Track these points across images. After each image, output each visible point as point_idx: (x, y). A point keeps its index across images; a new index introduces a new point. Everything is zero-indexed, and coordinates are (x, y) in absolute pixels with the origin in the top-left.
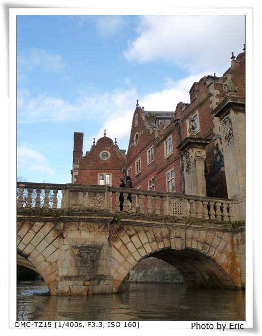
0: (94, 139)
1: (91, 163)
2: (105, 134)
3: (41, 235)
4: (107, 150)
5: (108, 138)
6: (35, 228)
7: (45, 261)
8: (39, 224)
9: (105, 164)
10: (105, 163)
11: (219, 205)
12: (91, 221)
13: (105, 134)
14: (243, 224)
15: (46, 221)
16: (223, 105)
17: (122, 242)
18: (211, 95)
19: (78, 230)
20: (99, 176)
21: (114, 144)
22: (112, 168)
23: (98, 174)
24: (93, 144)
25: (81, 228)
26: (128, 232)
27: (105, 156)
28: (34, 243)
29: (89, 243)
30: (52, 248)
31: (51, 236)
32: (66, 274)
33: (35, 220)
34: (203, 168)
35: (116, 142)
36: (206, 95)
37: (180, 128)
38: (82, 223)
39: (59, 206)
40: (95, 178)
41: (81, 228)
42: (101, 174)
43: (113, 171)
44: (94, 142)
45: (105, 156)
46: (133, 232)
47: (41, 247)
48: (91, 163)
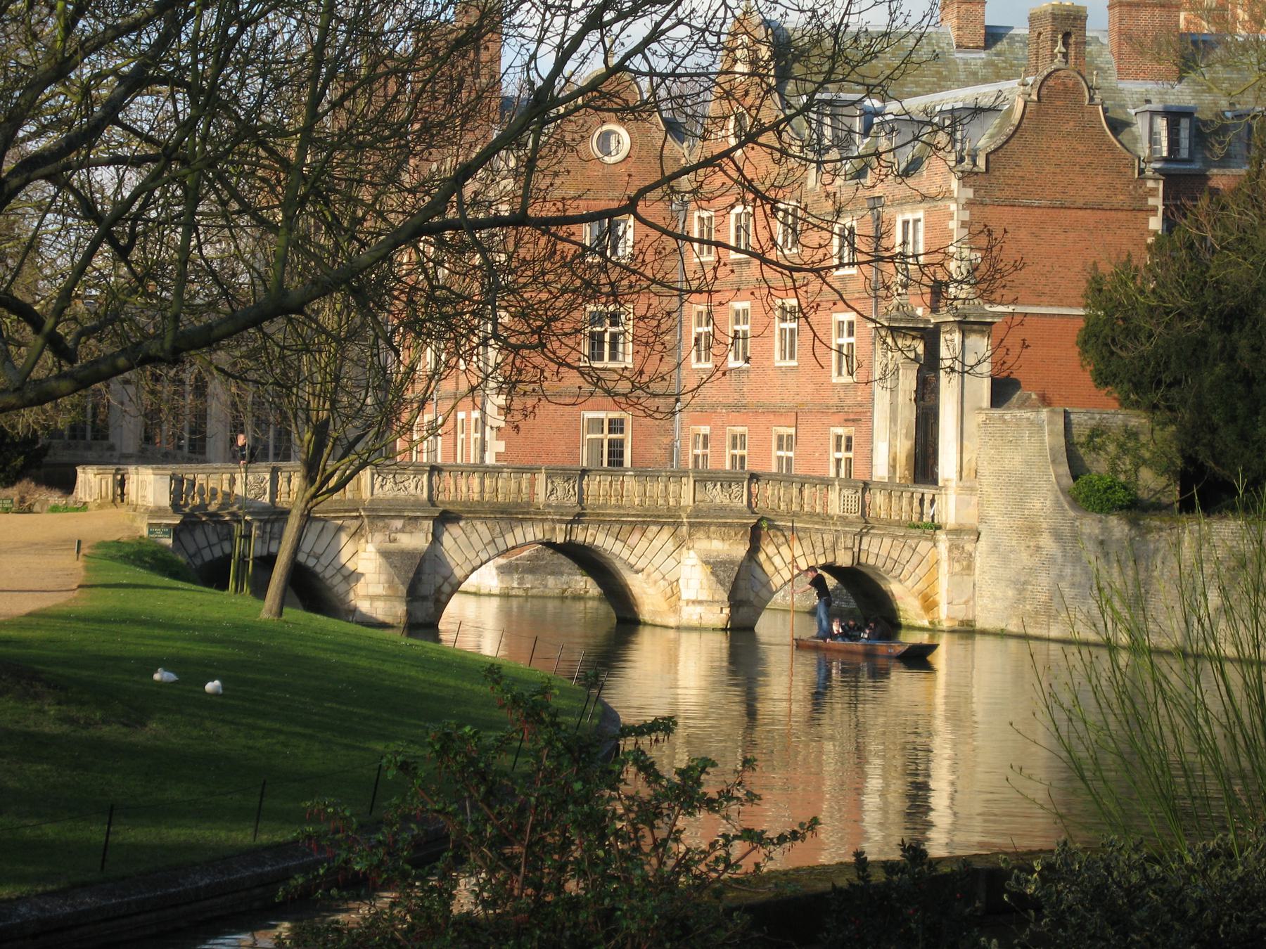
3: (657, 543)
6: (650, 535)
7: (664, 578)
8: (654, 529)
11: (917, 496)
14: (30, 510)
15: (663, 525)
17: (261, 802)
26: (775, 540)
28: (649, 555)
29: (723, 557)
30: (671, 562)
31: (670, 546)
32: (694, 598)
33: (648, 524)
34: (681, 667)
39: (472, 461)
47: (657, 561)
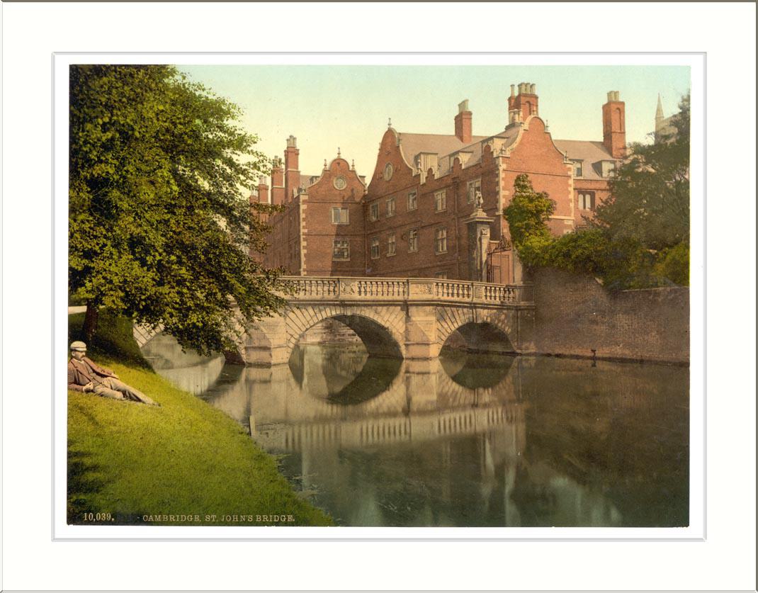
2: (339, 154)
13: (339, 154)
35: (353, 166)
44: (325, 165)
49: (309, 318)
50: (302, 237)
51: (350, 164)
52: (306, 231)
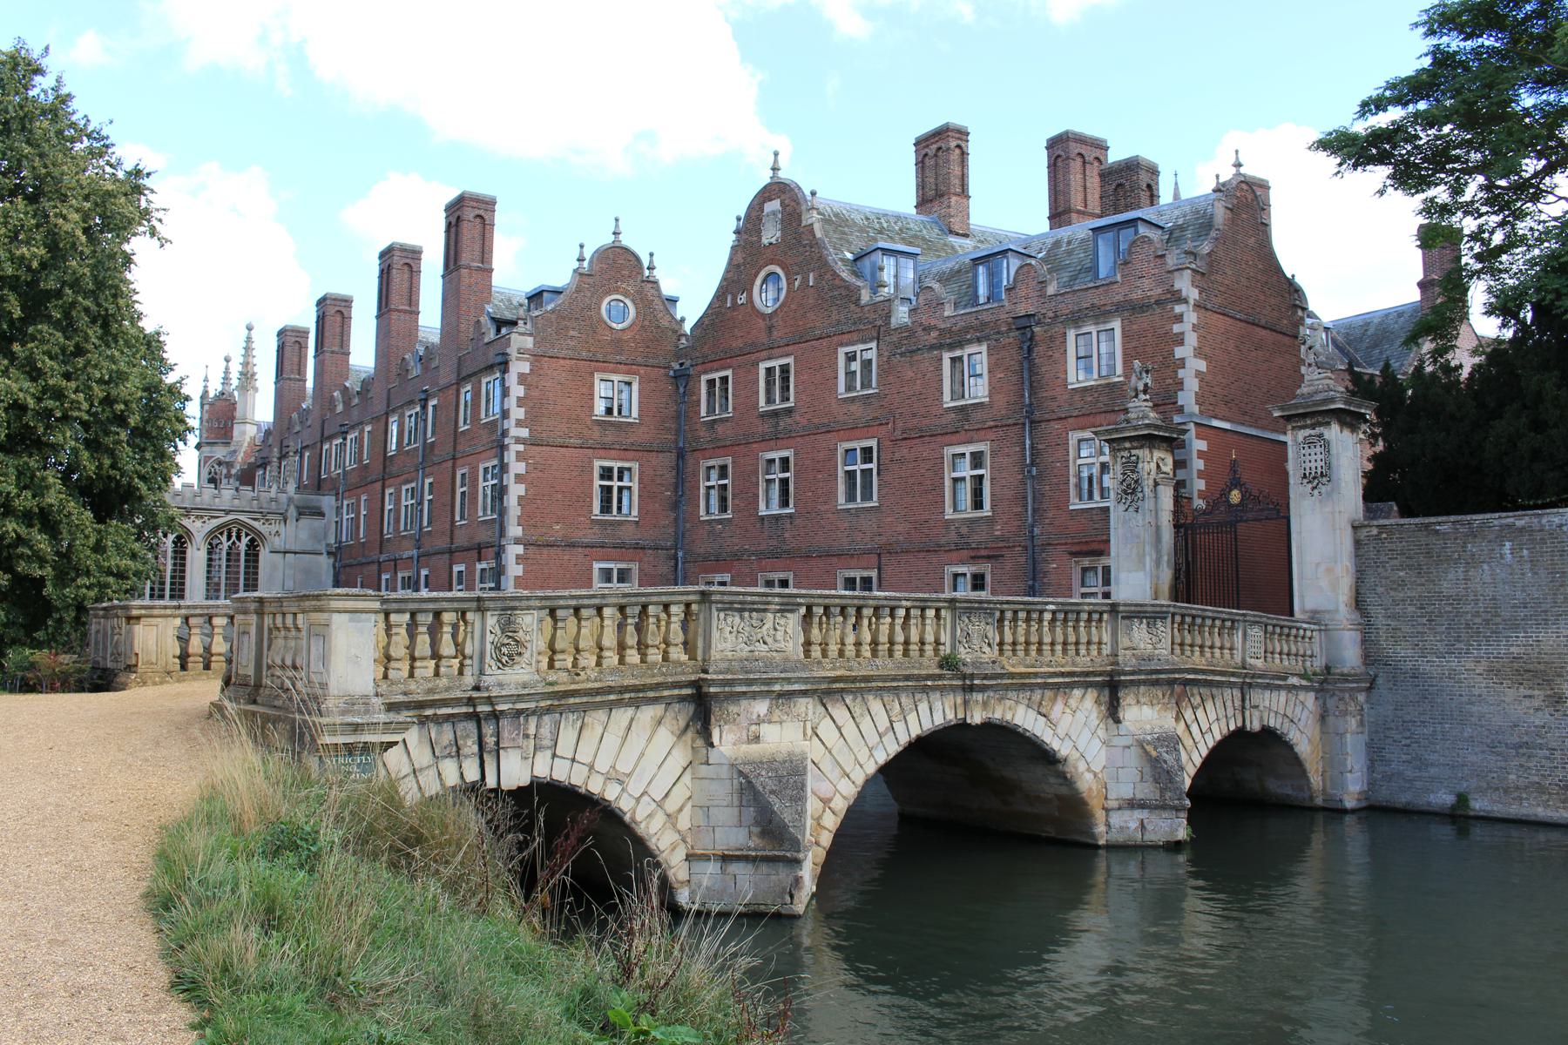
0: (582, 246)
1: (572, 333)
4: (626, 294)
5: (626, 250)
9: (617, 342)
10: (619, 340)
12: (1156, 683)
16: (1319, 405)
18: (1179, 298)
19: (1138, 702)
20: (597, 382)
21: (647, 273)
22: (639, 359)
23: (597, 376)
24: (576, 265)
25: (1143, 700)
27: (618, 312)
36: (1159, 291)
37: (1031, 339)
38: (1142, 689)
40: (584, 390)
41: (1143, 700)
42: (605, 376)
43: (642, 370)
44: (581, 260)
45: (618, 312)
46: (1196, 700)
48: (572, 333)
49: (873, 739)
50: (515, 448)
51: (646, 263)
52: (524, 433)
